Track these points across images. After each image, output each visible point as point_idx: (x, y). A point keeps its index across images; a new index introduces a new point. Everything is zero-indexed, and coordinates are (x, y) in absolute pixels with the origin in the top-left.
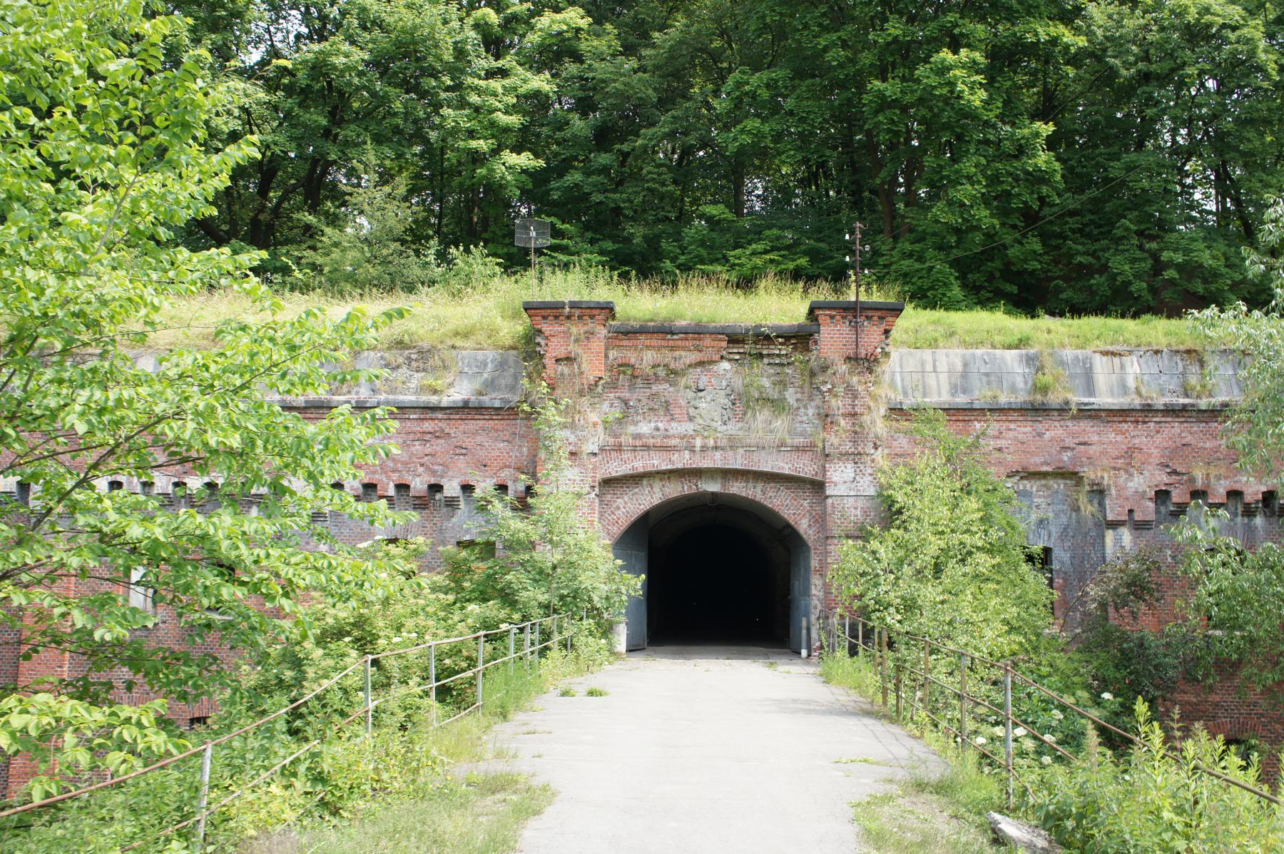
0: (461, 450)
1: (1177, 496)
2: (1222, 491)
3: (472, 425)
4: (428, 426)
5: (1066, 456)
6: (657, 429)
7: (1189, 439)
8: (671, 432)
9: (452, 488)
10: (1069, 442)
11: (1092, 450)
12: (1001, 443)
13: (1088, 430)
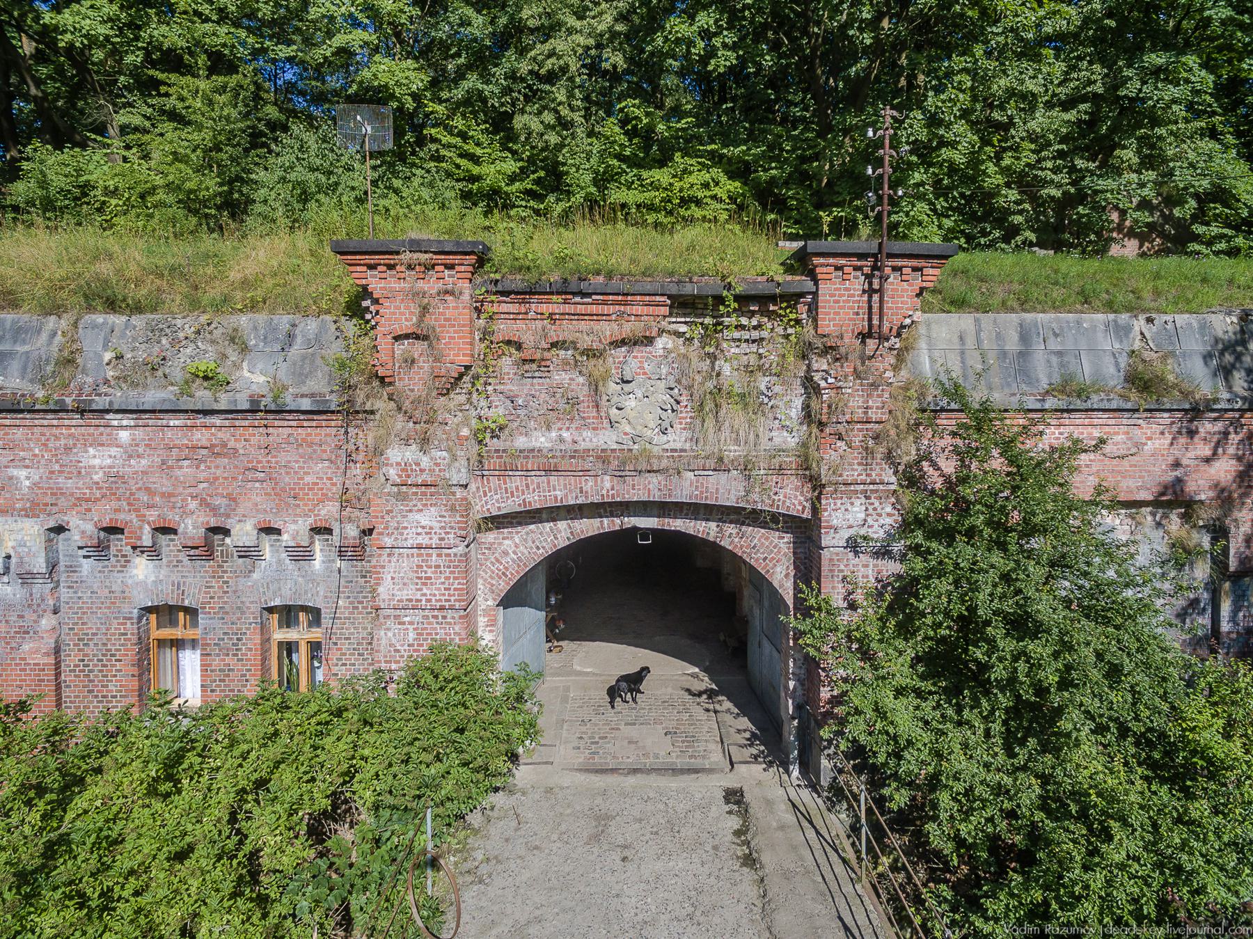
4: (201, 437)
6: (562, 440)
8: (583, 445)
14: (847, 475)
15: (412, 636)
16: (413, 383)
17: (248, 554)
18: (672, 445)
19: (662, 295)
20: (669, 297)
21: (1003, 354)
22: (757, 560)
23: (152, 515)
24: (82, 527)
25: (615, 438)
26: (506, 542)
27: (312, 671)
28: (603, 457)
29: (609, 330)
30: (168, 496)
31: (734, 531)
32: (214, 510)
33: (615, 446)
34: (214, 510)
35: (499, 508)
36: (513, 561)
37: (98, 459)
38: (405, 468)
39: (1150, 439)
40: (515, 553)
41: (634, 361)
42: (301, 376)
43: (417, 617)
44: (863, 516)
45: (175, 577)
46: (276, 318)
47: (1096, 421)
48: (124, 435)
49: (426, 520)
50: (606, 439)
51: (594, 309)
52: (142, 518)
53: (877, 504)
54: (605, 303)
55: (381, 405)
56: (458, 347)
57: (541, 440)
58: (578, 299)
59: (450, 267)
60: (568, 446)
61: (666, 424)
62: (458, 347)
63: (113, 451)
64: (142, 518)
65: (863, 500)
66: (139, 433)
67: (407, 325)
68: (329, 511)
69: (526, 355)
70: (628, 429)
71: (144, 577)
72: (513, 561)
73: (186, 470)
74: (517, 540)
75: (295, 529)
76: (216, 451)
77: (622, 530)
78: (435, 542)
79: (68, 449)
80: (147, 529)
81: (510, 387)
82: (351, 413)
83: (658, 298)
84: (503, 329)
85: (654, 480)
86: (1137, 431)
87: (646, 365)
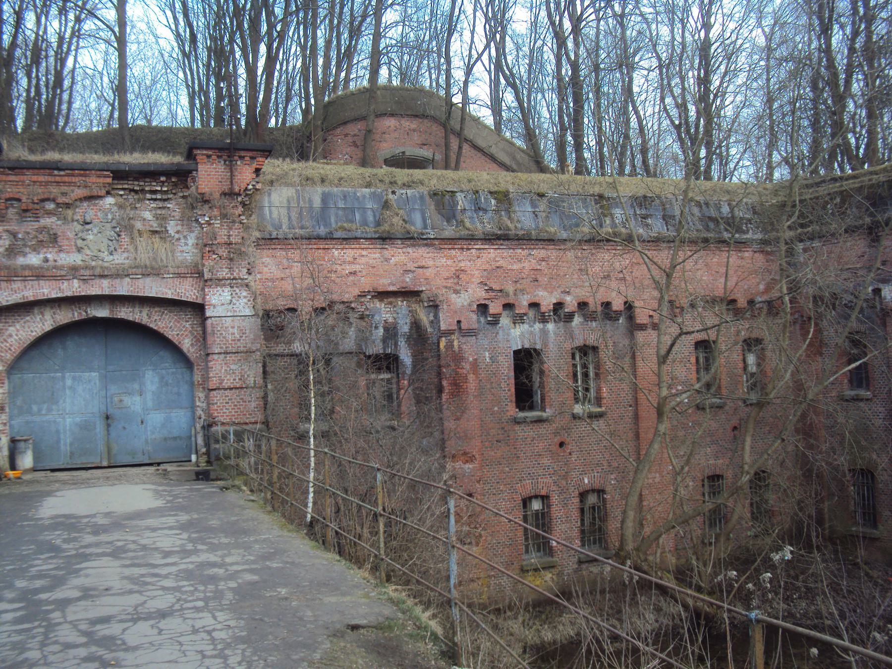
2: (525, 303)
5: (408, 278)
7: (501, 263)
8: (60, 263)
10: (411, 266)
11: (429, 273)
12: (357, 268)
13: (422, 254)
18: (117, 262)
19: (107, 171)
20: (112, 172)
22: (173, 335)
25: (80, 258)
26: (11, 328)
27: (203, 155)
29: (79, 192)
31: (157, 318)
33: (80, 263)
35: (7, 301)
36: (16, 340)
39: (393, 256)
40: (17, 335)
44: (230, 298)
47: (363, 246)
50: (75, 259)
51: (66, 179)
53: (238, 291)
54: (73, 175)
58: (56, 172)
60: (51, 263)
61: (112, 249)
65: (229, 289)
69: (24, 207)
70: (88, 252)
72: (16, 340)
74: (18, 327)
77: (170, 129)
83: (105, 173)
86: (385, 252)
87: (99, 214)
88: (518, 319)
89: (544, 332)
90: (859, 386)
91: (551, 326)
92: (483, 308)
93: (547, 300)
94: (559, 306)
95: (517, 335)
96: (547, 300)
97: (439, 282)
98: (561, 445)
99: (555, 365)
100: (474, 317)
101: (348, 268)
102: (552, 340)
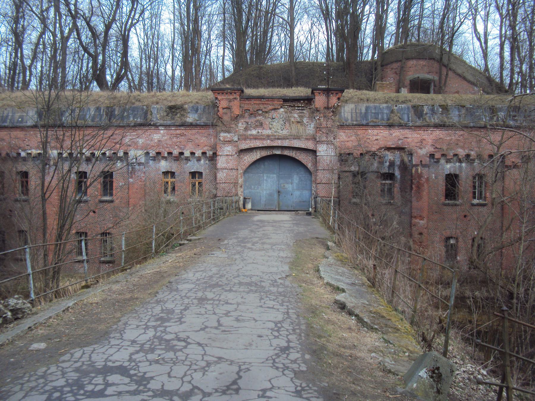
0: (189, 140)
1: (437, 156)
3: (194, 131)
4: (178, 132)
6: (258, 132)
8: (263, 133)
9: (187, 154)
10: (401, 137)
11: (409, 140)
12: (378, 137)
14: (323, 139)
15: (225, 175)
16: (226, 118)
17: (187, 159)
21: (361, 113)
23: (167, 149)
24: (152, 153)
28: (268, 136)
29: (271, 107)
30: (170, 145)
32: (181, 148)
34: (181, 148)
37: (156, 137)
38: (224, 137)
41: (274, 114)
42: (200, 118)
43: (226, 171)
45: (170, 165)
46: (357, 169)
48: (162, 131)
49: (228, 149)
50: (269, 132)
52: (165, 150)
55: (220, 124)
56: (237, 111)
57: (254, 132)
59: (235, 93)
62: (237, 111)
63: (160, 135)
64: (165, 150)
66: (165, 131)
67: (225, 106)
68: (205, 149)
71: (164, 165)
73: (175, 139)
75: (198, 153)
76: (182, 135)
78: (230, 154)
79: (150, 135)
80: (166, 153)
81: (247, 120)
82: (213, 126)
84: (246, 107)
85: (279, 141)
88: (448, 161)
89: (460, 167)
90: (105, 195)
91: (464, 165)
92: (432, 156)
93: (462, 153)
94: (468, 156)
95: (448, 168)
96: (462, 153)
97: (413, 144)
98: (465, 216)
99: (465, 184)
100: (428, 159)
101: (375, 138)
102: (464, 170)
